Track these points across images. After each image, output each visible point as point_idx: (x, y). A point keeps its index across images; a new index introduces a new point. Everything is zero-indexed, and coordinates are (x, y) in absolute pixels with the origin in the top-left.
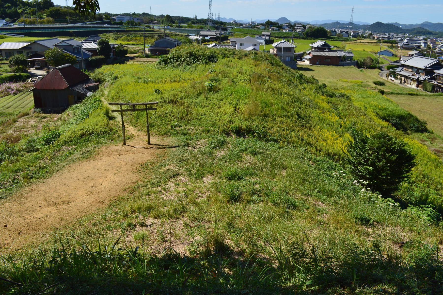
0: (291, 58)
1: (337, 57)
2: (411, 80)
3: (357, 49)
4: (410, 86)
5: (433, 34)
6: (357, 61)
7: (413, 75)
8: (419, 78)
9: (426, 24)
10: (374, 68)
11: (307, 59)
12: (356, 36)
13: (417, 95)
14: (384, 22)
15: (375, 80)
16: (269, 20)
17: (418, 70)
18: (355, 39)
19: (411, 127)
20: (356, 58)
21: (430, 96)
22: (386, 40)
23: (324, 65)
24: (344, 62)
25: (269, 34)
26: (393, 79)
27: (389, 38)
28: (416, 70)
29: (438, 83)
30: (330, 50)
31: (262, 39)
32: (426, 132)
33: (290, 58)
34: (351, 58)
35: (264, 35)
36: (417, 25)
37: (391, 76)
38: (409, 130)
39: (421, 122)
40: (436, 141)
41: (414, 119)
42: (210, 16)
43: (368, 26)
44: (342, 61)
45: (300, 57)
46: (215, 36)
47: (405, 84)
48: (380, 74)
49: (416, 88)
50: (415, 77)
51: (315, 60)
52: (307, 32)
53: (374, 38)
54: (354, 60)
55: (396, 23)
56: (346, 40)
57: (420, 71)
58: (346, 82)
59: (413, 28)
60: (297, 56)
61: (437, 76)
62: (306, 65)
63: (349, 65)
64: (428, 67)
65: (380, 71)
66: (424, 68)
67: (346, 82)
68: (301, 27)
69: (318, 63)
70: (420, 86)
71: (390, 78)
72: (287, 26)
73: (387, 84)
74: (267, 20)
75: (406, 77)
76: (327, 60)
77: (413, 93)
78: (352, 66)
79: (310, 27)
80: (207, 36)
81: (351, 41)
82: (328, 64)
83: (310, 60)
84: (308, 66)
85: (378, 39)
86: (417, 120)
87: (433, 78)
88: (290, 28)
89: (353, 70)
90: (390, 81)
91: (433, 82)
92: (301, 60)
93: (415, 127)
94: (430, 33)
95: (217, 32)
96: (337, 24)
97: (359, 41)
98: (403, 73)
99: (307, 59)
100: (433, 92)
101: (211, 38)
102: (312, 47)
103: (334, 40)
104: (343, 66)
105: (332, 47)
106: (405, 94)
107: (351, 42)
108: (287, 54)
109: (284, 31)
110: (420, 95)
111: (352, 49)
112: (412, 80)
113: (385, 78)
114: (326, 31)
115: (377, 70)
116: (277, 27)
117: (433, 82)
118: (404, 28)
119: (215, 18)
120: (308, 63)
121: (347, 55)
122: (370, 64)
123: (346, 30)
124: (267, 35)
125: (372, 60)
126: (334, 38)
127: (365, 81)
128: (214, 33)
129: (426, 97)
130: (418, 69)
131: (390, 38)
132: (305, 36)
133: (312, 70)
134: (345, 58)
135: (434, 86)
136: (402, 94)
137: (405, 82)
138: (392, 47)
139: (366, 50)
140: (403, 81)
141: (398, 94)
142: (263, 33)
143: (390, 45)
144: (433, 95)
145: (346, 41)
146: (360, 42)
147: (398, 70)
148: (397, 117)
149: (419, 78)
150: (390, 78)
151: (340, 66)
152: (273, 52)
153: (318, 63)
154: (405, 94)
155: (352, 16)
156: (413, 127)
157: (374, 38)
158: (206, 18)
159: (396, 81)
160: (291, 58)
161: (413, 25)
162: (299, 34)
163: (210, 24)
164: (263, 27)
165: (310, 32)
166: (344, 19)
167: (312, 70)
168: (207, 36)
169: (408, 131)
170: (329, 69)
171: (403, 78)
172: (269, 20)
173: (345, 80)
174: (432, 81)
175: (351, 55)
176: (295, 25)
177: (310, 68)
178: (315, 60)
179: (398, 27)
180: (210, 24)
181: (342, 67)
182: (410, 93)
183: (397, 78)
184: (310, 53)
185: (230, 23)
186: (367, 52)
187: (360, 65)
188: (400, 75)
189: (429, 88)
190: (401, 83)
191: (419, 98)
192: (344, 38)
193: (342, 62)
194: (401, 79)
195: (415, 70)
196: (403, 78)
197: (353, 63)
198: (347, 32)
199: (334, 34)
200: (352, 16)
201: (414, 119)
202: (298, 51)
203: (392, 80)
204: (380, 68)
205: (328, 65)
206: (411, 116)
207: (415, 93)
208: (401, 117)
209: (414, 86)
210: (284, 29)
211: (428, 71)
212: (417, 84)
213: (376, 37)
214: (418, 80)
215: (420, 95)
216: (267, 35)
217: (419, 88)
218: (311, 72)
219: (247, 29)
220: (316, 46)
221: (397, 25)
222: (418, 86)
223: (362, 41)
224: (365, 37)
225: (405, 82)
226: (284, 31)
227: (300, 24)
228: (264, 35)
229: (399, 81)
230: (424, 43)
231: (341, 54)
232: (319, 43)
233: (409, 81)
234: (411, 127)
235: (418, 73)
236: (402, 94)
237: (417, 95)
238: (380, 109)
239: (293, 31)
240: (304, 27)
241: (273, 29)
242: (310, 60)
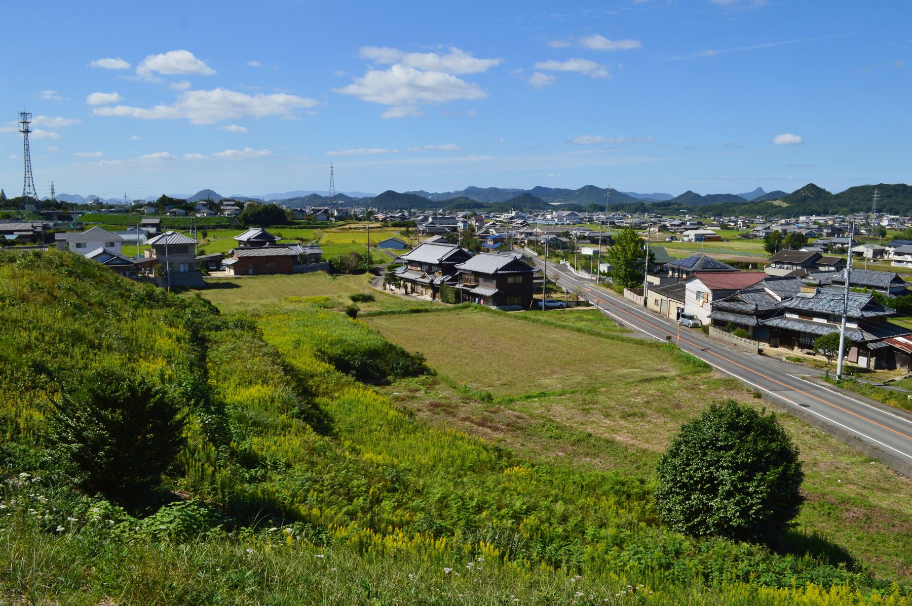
0: (191, 265)
1: (287, 256)
2: (422, 286)
3: (340, 242)
4: (422, 297)
5: (483, 207)
6: (330, 261)
7: (424, 277)
8: (432, 281)
9: (472, 190)
10: (362, 272)
11: (229, 266)
12: (344, 217)
13: (427, 311)
14: (401, 190)
15: (354, 293)
16: (164, 196)
17: (429, 268)
18: (340, 223)
19: (393, 369)
20: (328, 255)
21: (449, 310)
22: (398, 220)
23: (264, 274)
24: (304, 266)
25: (157, 221)
26: (393, 287)
27: (403, 217)
28: (427, 267)
29: (465, 286)
30: (274, 244)
31: (141, 232)
32: (423, 374)
33: (187, 266)
34: (317, 258)
35: (145, 225)
36: (457, 193)
37: (389, 283)
38: (390, 374)
39: (412, 358)
40: (437, 387)
41: (397, 353)
42: (27, 190)
43: (371, 199)
44: (299, 264)
45: (217, 263)
46: (31, 233)
47: (414, 294)
48: (374, 281)
49: (431, 299)
50: (427, 281)
51: (243, 267)
52: (245, 215)
53: (377, 220)
54: (324, 261)
55: (422, 192)
56: (324, 226)
57: (434, 269)
58: (296, 301)
59: (450, 198)
60: (208, 262)
61: (461, 274)
62: (227, 278)
63: (313, 269)
64: (446, 260)
65: (373, 276)
66: (437, 262)
67: (296, 301)
68: (233, 205)
69: (251, 271)
70: (438, 295)
71: (388, 286)
72: (204, 205)
73: (377, 297)
74: (161, 196)
75: (413, 282)
76: (268, 265)
77: (421, 308)
78: (320, 272)
79: (249, 205)
80: (11, 232)
81: (333, 227)
82: (272, 272)
83: (234, 266)
84: (232, 278)
85: (383, 220)
86: (404, 354)
87: (455, 279)
88: (211, 209)
89: (321, 279)
90: (390, 292)
91: (457, 286)
92: (218, 269)
93: (401, 368)
94: (479, 206)
95: (34, 224)
96: (314, 198)
97: (347, 226)
98: (407, 275)
99: (229, 266)
100: (459, 302)
101: (20, 237)
102: (240, 242)
103: (300, 228)
104: (302, 272)
105: (277, 239)
106: (405, 313)
107: (333, 230)
108: (177, 258)
109: (199, 215)
110: (432, 311)
111: (337, 241)
112: (423, 285)
113: (379, 288)
114: (282, 212)
115: (367, 276)
116: (183, 208)
117: (457, 286)
118: (435, 199)
119: (43, 194)
120: (230, 273)
121: (309, 251)
122: (354, 264)
123: (323, 208)
124: (153, 225)
125: (359, 257)
126: (301, 223)
127: (336, 296)
128: (27, 226)
129: (443, 314)
130: (430, 265)
131: (406, 218)
132: (242, 224)
133: (237, 286)
134: (304, 258)
135: (457, 292)
136: (400, 312)
137: (413, 291)
138: (407, 234)
139: (357, 241)
140: (409, 290)
141: (393, 313)
142: (144, 221)
143: (404, 229)
144: (454, 309)
145: (323, 228)
146: (351, 228)
147: (399, 272)
148: (365, 353)
149: (432, 281)
150: (388, 286)
151: (297, 273)
152: (151, 256)
153: (251, 271)
154: (405, 313)
155: (332, 182)
156: (396, 369)
157: (377, 220)
158: (20, 195)
159: (397, 291)
160: (191, 265)
161: (449, 193)
162: (229, 219)
163: (29, 209)
164: (153, 210)
165: (252, 215)
166: (323, 188)
167: (237, 286)
168: (11, 232)
169: (389, 378)
170: (272, 281)
171: (409, 285)
172: (164, 196)
173: (295, 298)
174: (455, 285)
175: (316, 251)
176: (221, 203)
177: (237, 282)
178: (243, 267)
179: (424, 198)
180: (29, 209)
181: (299, 275)
182: (414, 308)
183: (399, 286)
184: (233, 254)
185: (87, 205)
186: (360, 245)
187: (335, 269)
188: (402, 278)
189: (451, 296)
190: (407, 293)
191: (429, 316)
192: (319, 222)
193: (300, 267)
194: (406, 288)
195: (425, 268)
196: (409, 285)
197: (322, 266)
198: (326, 212)
199: (300, 215)
200: (332, 182)
201: (397, 353)
202: (212, 251)
203: (392, 290)
204: (376, 272)
205: (272, 274)
206: (392, 348)
207: (423, 308)
208: (373, 353)
209: (427, 296)
210: (198, 211)
211: (447, 267)
212: (431, 291)
213: (380, 216)
214: (431, 285)
215: (432, 311)
216: (153, 225)
217: (436, 299)
218: (235, 289)
219: (117, 214)
220: (245, 240)
221: (422, 196)
222: (434, 296)
223: (353, 226)
224: (360, 220)
225: (413, 291)
226: (199, 215)
227: (233, 200)
228: (145, 225)
229: (403, 291)
230: (463, 222)
231: (298, 250)
232: (252, 233)
233: (419, 289)
234: (393, 369)
235: (430, 272)
236: (400, 312)
237: (427, 311)
238: (331, 344)
239: (216, 214)
240: (240, 205)
241: (175, 212)
242: (234, 266)
